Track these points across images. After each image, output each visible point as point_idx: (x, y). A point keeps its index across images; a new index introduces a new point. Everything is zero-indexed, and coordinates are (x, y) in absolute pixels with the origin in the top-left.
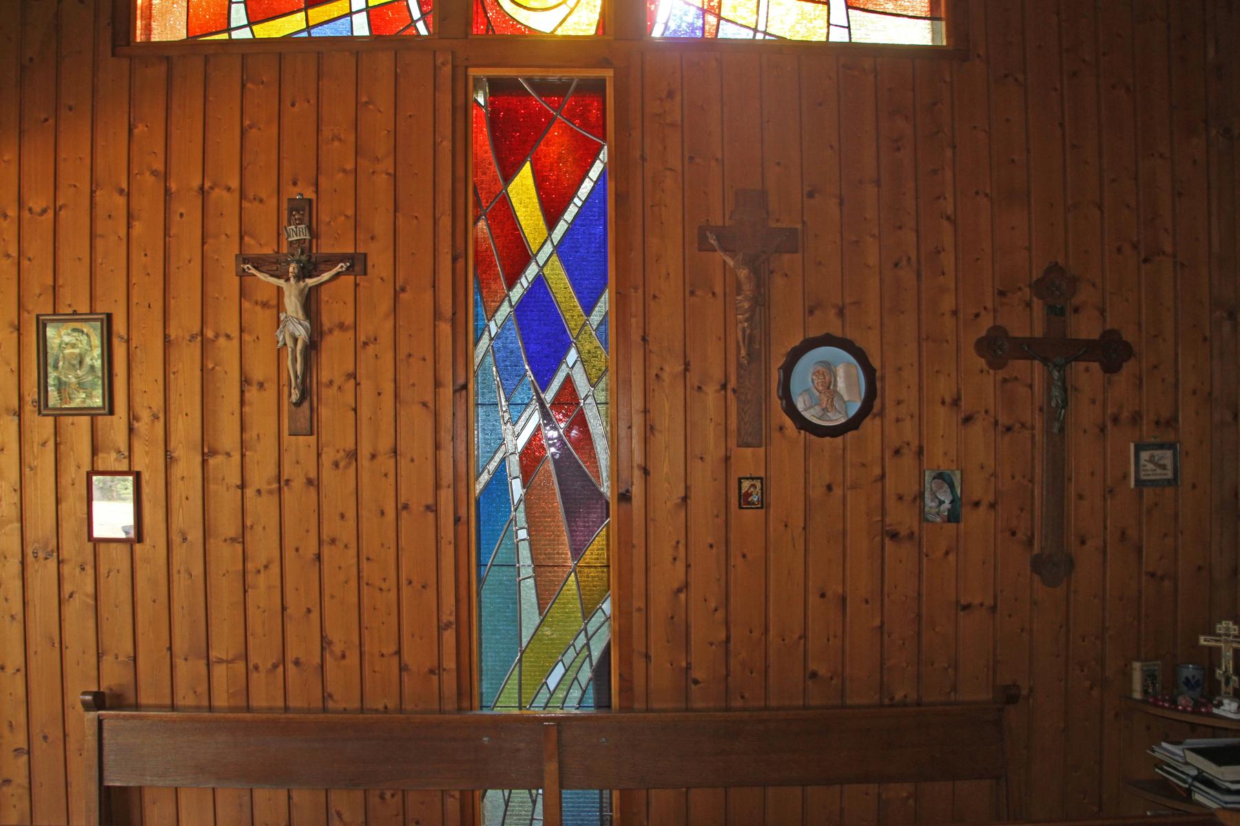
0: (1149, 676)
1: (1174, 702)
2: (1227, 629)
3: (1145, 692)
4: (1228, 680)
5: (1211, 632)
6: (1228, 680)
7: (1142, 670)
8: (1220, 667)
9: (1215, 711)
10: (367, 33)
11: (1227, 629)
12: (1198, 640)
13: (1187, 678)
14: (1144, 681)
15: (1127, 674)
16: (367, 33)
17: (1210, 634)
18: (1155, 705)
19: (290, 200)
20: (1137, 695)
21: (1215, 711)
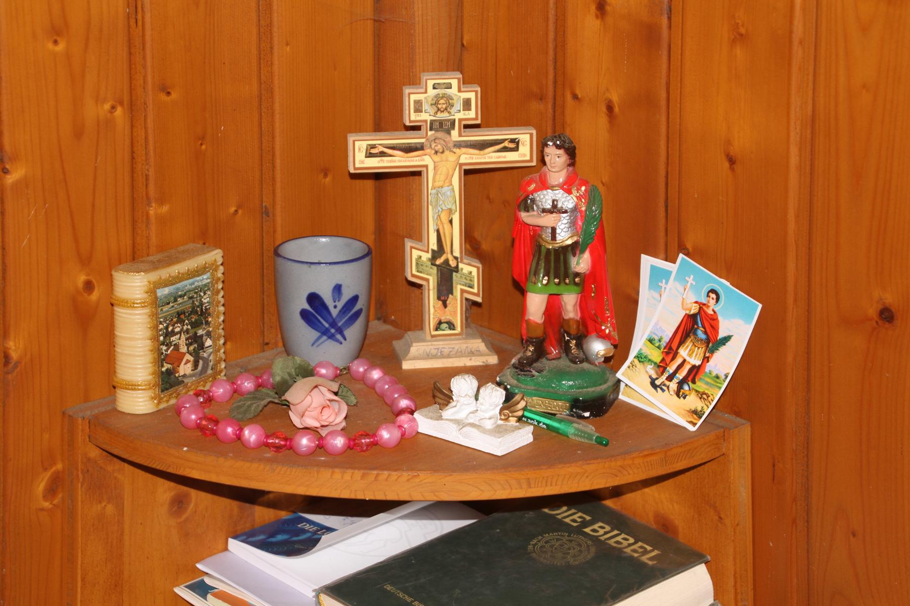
0: (183, 318)
1: (275, 406)
2: (443, 103)
3: (167, 381)
4: (446, 276)
5: (386, 117)
6: (446, 276)
7: (156, 303)
8: (417, 234)
9: (426, 424)
10: (643, 255)
11: (443, 103)
12: (343, 153)
13: (314, 299)
14: (162, 337)
15: (94, 323)
16: (643, 255)
17: (379, 127)
18: (207, 432)
19: (675, 263)
20: (138, 403)
21: (426, 424)
